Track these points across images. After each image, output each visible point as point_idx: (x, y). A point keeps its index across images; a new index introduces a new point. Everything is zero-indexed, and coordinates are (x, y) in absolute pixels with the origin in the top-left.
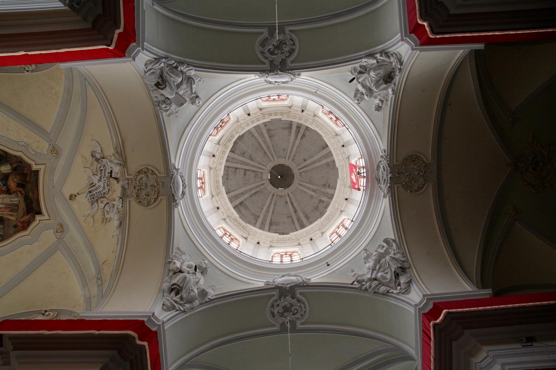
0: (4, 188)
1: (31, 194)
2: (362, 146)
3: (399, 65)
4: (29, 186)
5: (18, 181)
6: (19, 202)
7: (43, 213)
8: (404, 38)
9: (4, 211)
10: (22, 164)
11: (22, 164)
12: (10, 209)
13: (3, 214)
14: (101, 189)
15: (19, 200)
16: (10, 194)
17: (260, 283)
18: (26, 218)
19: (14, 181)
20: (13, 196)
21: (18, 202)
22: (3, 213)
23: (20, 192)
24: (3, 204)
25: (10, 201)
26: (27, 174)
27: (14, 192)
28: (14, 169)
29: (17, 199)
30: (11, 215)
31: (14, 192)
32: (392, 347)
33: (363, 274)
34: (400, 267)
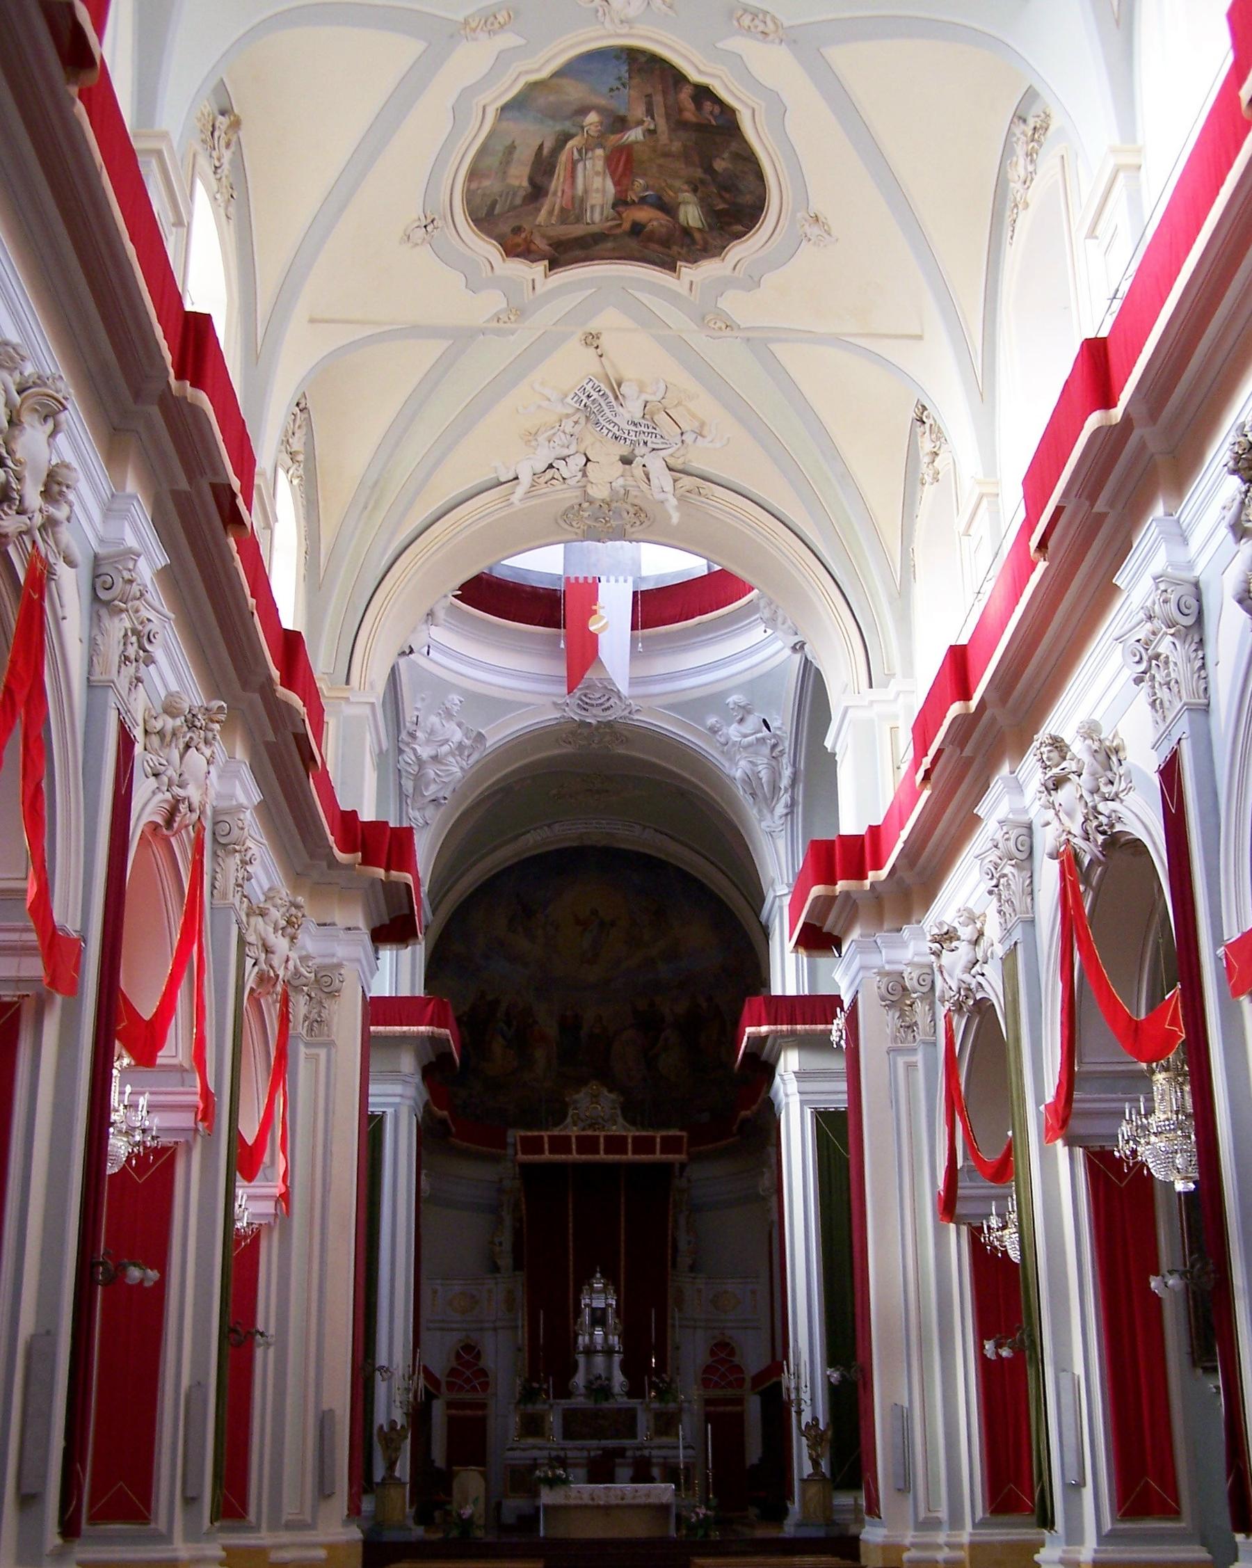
0: (632, 196)
1: (610, 245)
2: (1229, 917)
3: (566, 1122)
4: (633, 244)
5: (649, 227)
6: (588, 224)
7: (552, 272)
8: (684, 1134)
9: (565, 197)
10: (699, 250)
11: (699, 250)
12: (570, 208)
13: (555, 193)
14: (609, 414)
15: (593, 223)
16: (614, 206)
17: (180, 291)
18: (541, 244)
19: (650, 220)
20: (609, 211)
21: (589, 221)
22: (559, 194)
23: (619, 225)
24: (586, 191)
25: (593, 207)
26: (669, 248)
27: (619, 214)
28: (687, 232)
29: (597, 217)
30: (551, 212)
31: (619, 214)
32: (558, 1128)
33: (483, 1373)
34: (983, 1008)
